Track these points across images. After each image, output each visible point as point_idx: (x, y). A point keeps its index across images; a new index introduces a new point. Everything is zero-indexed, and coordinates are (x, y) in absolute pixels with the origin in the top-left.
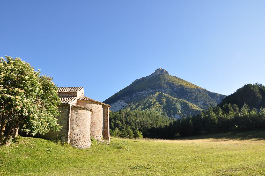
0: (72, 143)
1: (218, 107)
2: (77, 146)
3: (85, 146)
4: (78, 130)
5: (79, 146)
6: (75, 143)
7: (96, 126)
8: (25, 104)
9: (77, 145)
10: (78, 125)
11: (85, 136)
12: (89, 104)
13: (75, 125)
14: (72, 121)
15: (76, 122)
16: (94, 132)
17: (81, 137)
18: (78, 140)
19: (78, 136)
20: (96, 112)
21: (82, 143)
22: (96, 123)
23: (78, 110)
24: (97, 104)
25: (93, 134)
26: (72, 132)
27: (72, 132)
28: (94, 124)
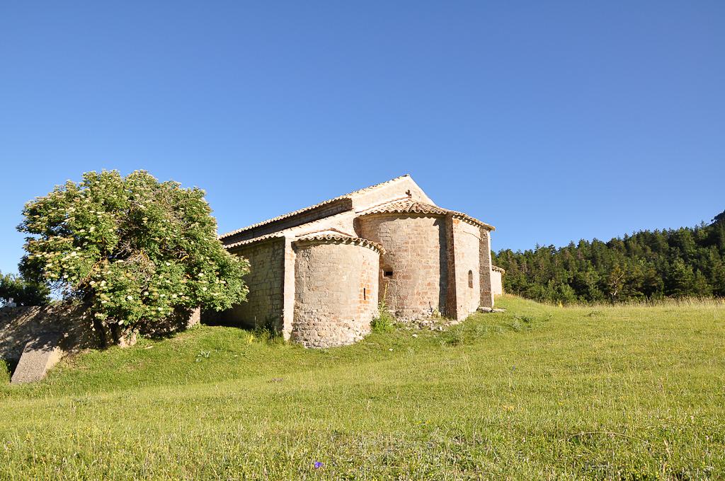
0: (297, 335)
1: (42, 302)
2: (305, 343)
3: (331, 342)
4: (315, 299)
5: (313, 341)
6: (303, 335)
7: (411, 280)
8: (64, 266)
9: (306, 340)
10: (312, 286)
11: (337, 315)
12: (386, 223)
13: (305, 288)
14: (298, 279)
15: (308, 279)
16: (405, 297)
17: (321, 318)
18: (312, 326)
19: (313, 317)
20: (410, 241)
21: (323, 333)
22: (413, 271)
23: (313, 248)
24: (422, 217)
25: (402, 304)
26: (298, 308)
27: (298, 308)
28: (404, 277)
